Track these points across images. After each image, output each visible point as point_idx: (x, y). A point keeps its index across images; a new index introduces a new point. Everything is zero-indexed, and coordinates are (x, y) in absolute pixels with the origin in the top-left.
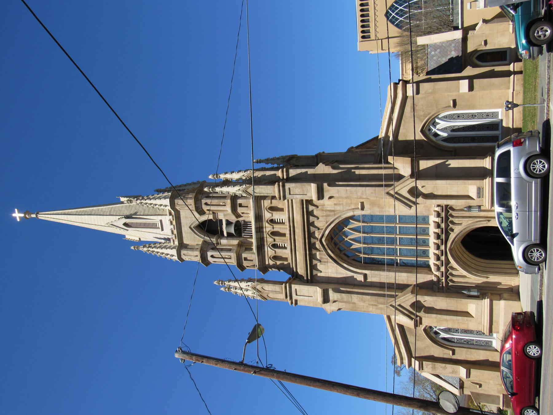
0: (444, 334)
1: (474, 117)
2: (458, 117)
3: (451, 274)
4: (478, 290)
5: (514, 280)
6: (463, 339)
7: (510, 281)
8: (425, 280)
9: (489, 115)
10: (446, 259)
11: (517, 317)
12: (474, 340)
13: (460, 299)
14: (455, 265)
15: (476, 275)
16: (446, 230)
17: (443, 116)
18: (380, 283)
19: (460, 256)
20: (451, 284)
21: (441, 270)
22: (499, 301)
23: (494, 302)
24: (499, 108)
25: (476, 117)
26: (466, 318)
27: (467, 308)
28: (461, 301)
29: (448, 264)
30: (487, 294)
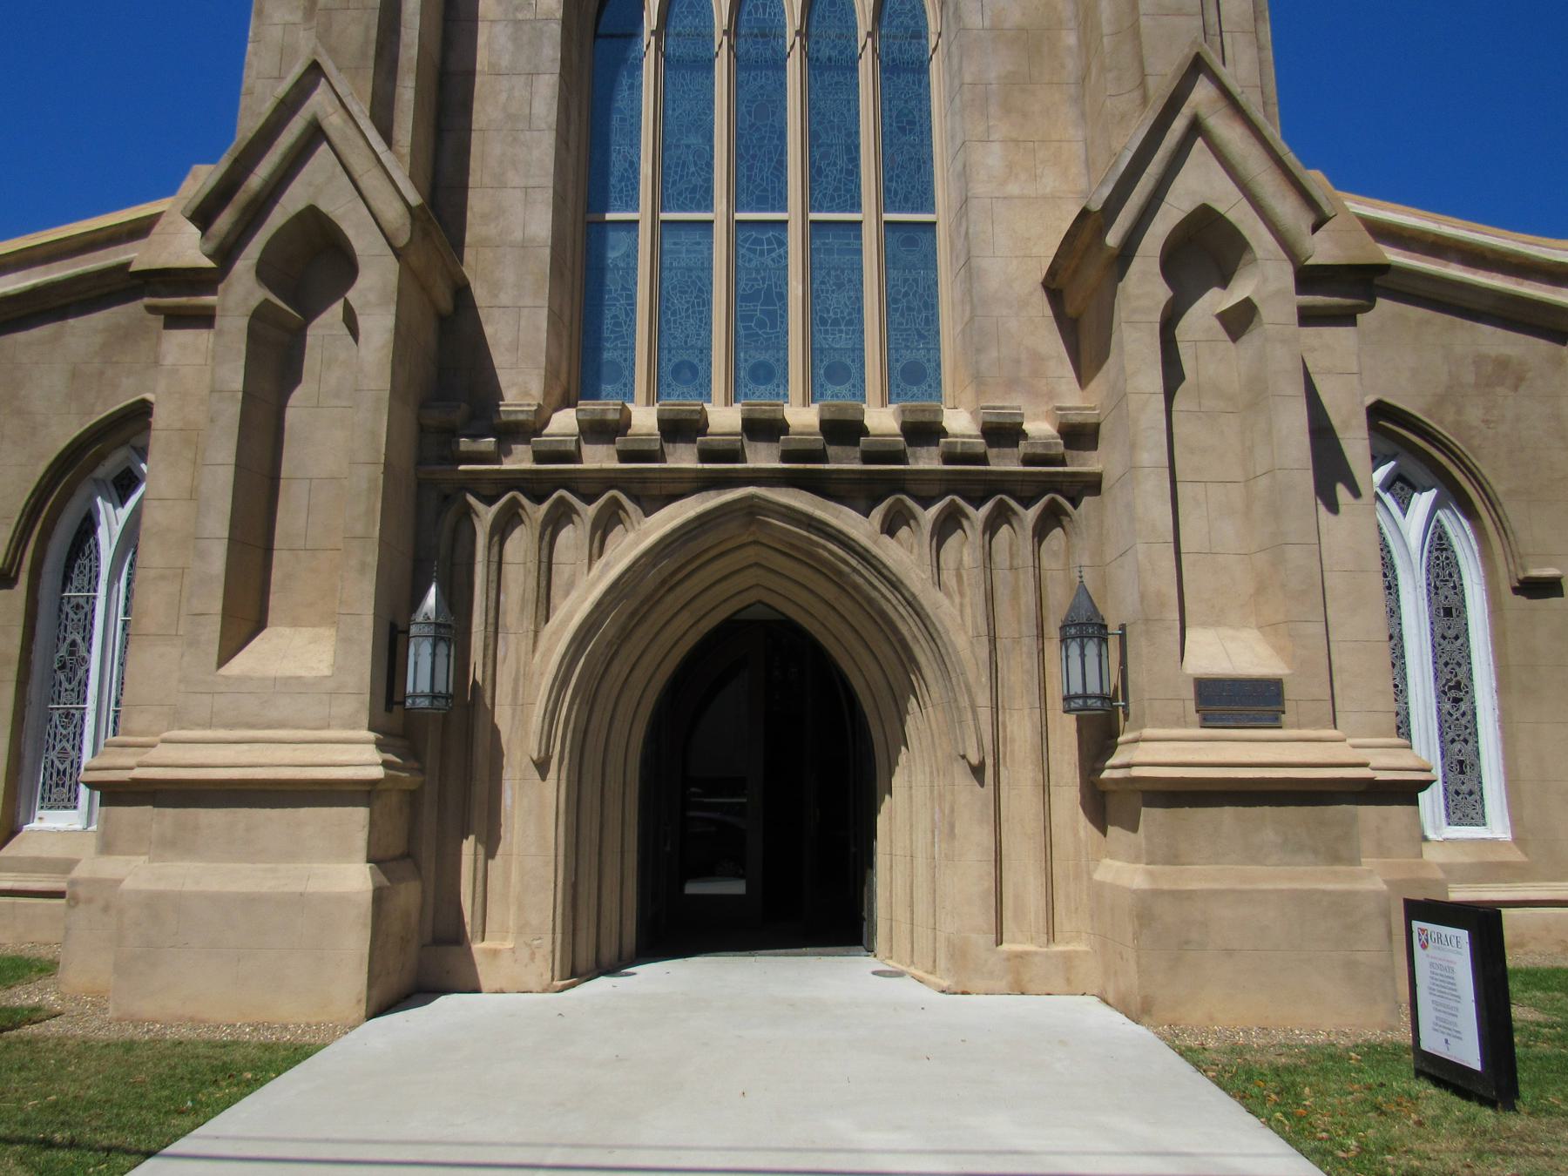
0: (118, 529)
1: (1453, 694)
2: (1448, 612)
3: (559, 518)
4: (447, 697)
5: (524, 954)
6: (88, 640)
7: (522, 929)
8: (500, 358)
9: (1462, 772)
10: (681, 480)
11: (499, 443)
12: (85, 700)
13: (373, 559)
14: (637, 543)
15: (561, 681)
16: (896, 483)
17: (1445, 533)
18: (471, 73)
19: (688, 584)
20: (486, 515)
21: (588, 450)
22: (363, 854)
23: (360, 814)
24: (1516, 821)
25: (1448, 706)
26: (217, 606)
27: (295, 622)
28: (363, 567)
29: (636, 499)
30: (416, 765)
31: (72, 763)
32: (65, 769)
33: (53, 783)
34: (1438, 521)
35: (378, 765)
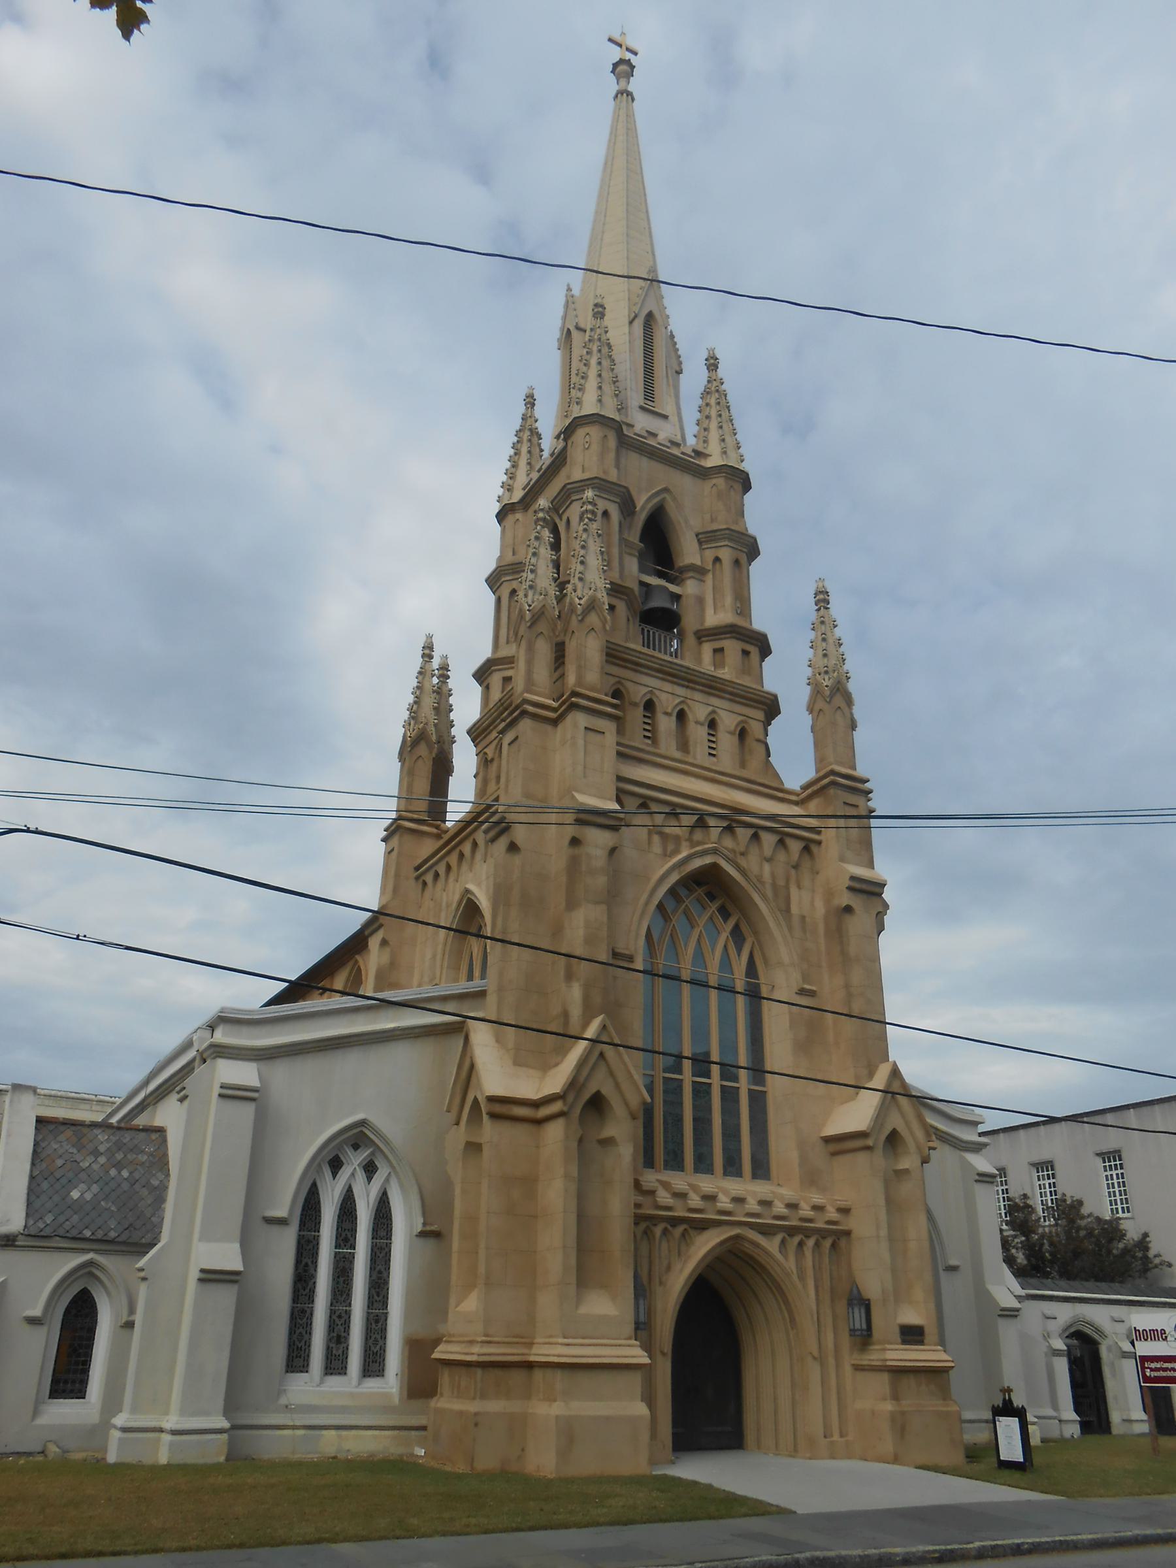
31: (306, 1342)
32: (301, 1347)
33: (371, 1360)
34: (359, 966)
35: (537, 1343)
